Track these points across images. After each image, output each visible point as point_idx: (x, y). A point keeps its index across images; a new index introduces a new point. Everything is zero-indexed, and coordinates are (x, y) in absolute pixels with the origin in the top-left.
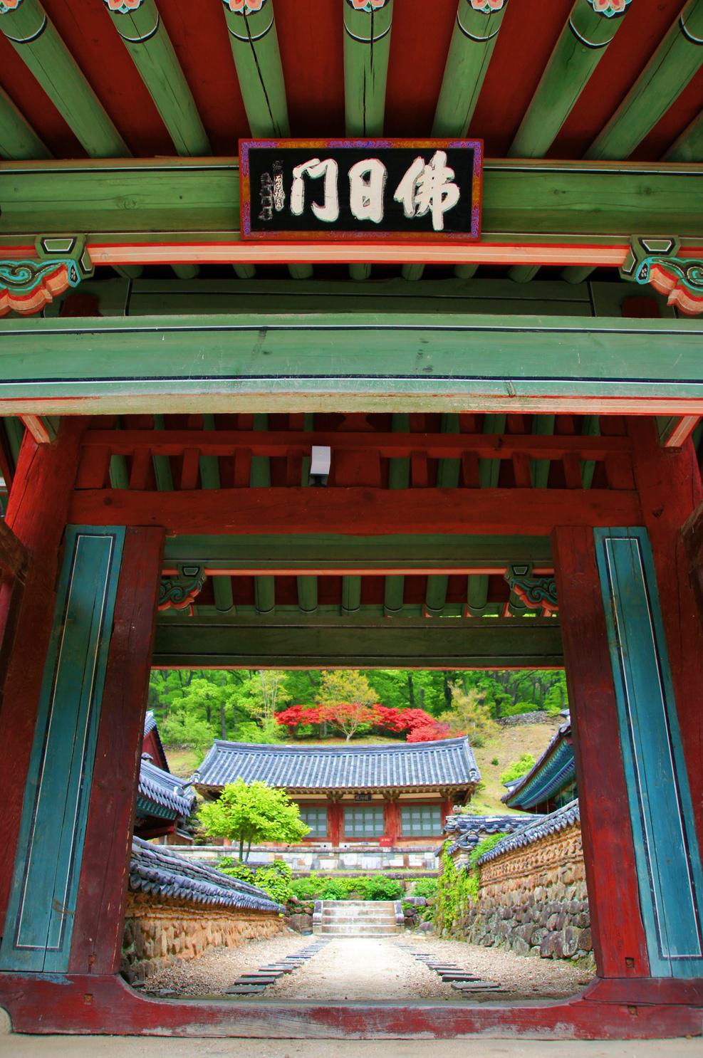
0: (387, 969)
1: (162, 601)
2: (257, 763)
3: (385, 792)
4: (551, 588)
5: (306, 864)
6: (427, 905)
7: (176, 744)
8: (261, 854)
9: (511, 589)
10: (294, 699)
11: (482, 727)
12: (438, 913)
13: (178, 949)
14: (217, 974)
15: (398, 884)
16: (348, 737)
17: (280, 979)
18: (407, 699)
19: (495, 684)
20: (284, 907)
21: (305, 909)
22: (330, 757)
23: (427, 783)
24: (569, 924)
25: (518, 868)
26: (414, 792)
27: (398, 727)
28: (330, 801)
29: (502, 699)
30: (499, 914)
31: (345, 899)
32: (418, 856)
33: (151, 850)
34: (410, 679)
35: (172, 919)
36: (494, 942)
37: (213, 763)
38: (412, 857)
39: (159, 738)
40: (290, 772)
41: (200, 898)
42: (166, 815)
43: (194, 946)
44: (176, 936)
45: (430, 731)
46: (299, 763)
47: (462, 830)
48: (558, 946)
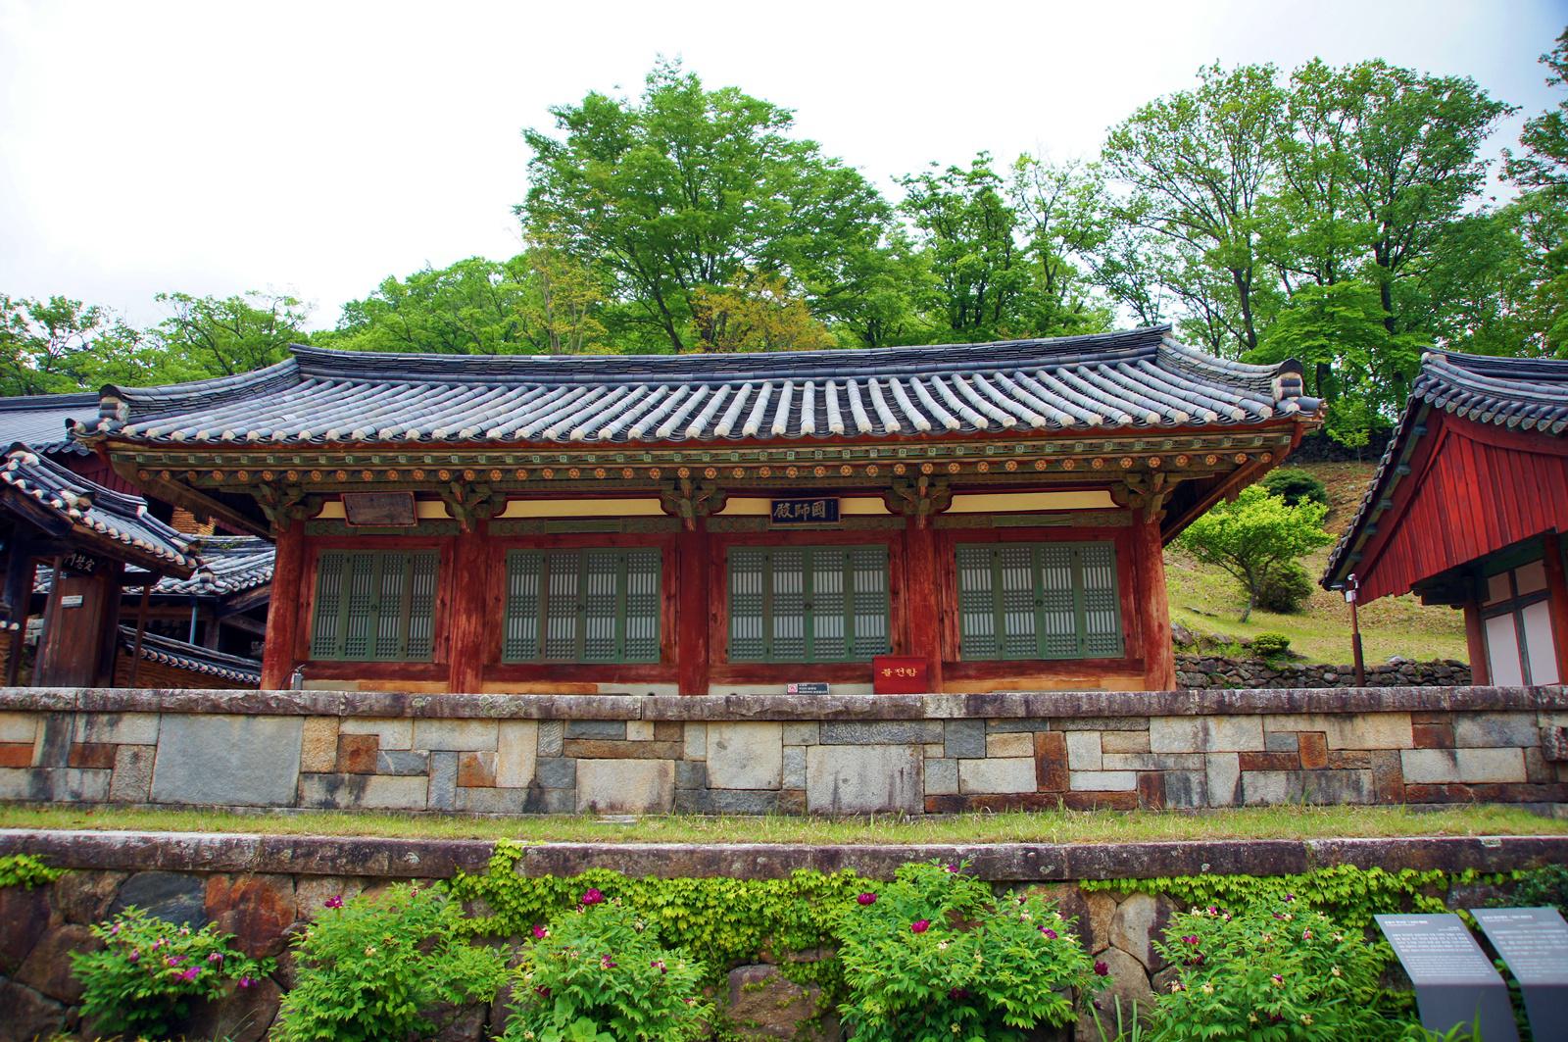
5: (501, 781)
28: (674, 526)
32: (1114, 740)
38: (1081, 745)
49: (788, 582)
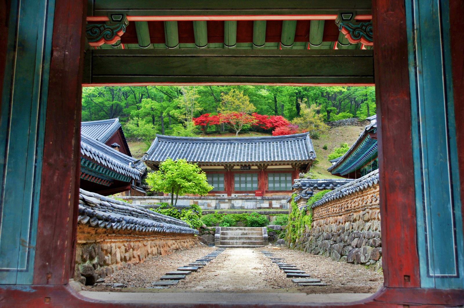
0: (255, 268)
1: (98, 39)
2: (182, 148)
3: (258, 165)
4: (368, 29)
5: (212, 206)
6: (281, 230)
7: (135, 138)
8: (185, 200)
9: (340, 30)
10: (205, 110)
11: (318, 127)
12: (288, 234)
13: (128, 258)
14: (151, 273)
15: (266, 217)
16: (237, 133)
17: (189, 276)
18: (273, 110)
19: (327, 101)
20: (198, 231)
21: (211, 232)
22: (226, 144)
23: (284, 159)
24: (365, 245)
25: (336, 211)
26: (276, 165)
27: (267, 127)
29: (331, 110)
30: (323, 236)
31: (234, 226)
32: (277, 202)
33: (108, 201)
34: (275, 98)
35: (123, 242)
36: (320, 252)
37: (156, 148)
39: (123, 134)
40: (202, 153)
41: (141, 229)
42: (124, 179)
43: (139, 256)
44: (126, 251)
45: (286, 129)
46: (208, 147)
47: (303, 187)
48: (358, 256)
49: (243, 179)
